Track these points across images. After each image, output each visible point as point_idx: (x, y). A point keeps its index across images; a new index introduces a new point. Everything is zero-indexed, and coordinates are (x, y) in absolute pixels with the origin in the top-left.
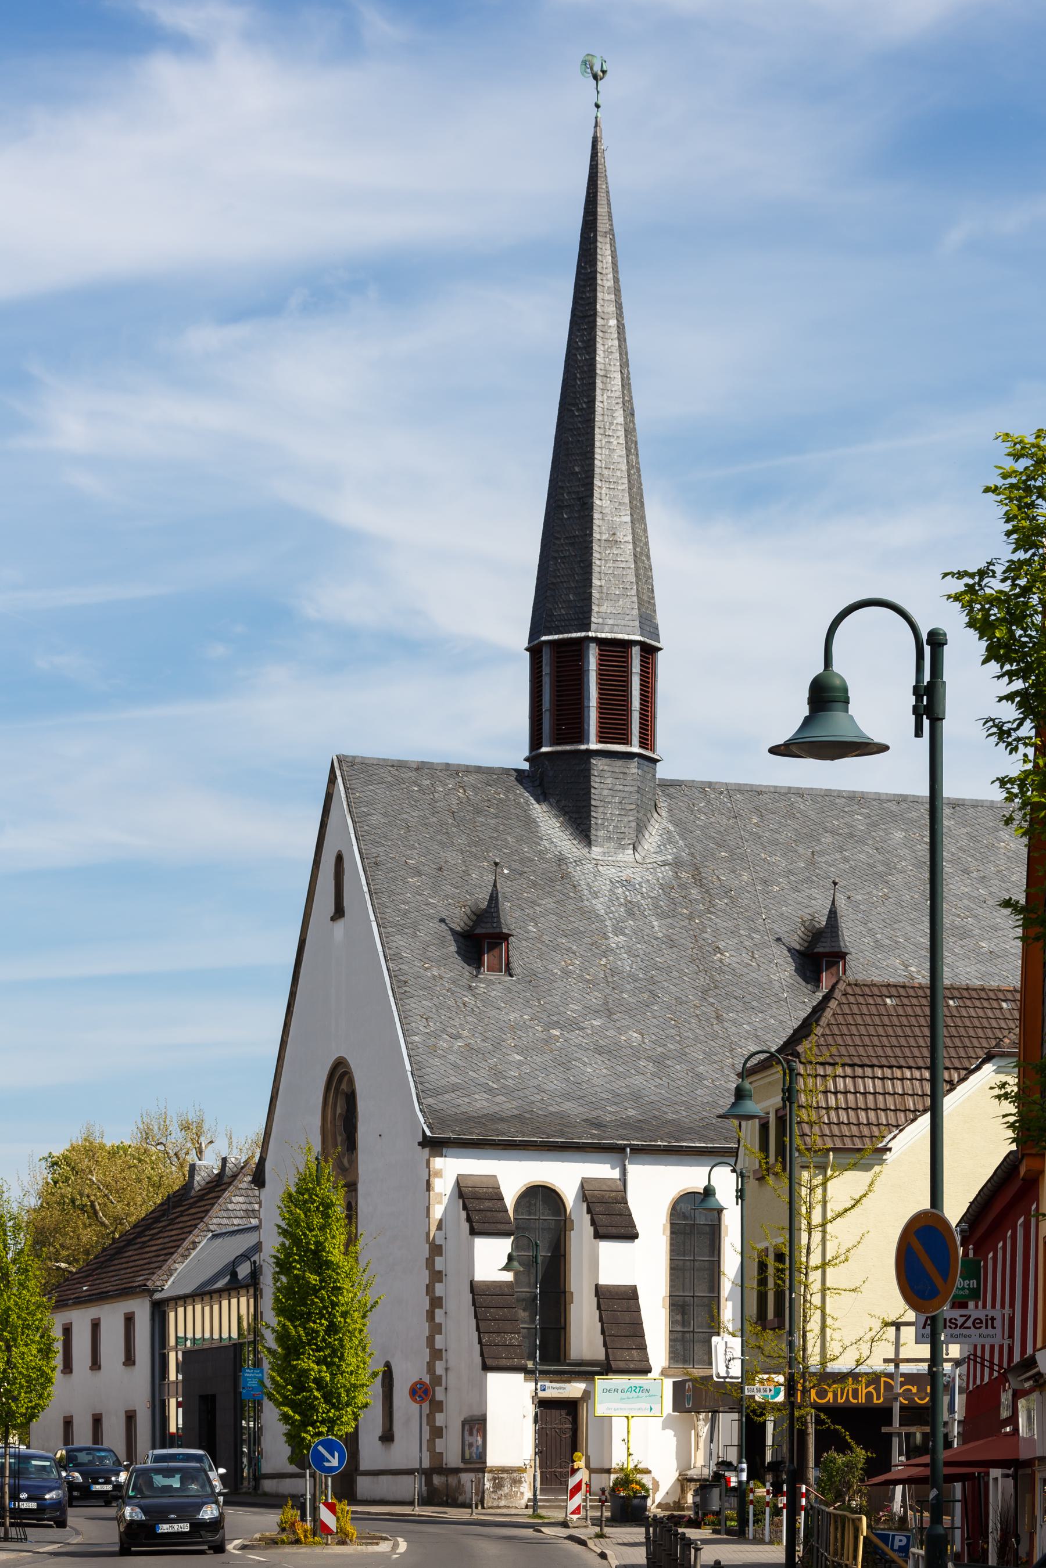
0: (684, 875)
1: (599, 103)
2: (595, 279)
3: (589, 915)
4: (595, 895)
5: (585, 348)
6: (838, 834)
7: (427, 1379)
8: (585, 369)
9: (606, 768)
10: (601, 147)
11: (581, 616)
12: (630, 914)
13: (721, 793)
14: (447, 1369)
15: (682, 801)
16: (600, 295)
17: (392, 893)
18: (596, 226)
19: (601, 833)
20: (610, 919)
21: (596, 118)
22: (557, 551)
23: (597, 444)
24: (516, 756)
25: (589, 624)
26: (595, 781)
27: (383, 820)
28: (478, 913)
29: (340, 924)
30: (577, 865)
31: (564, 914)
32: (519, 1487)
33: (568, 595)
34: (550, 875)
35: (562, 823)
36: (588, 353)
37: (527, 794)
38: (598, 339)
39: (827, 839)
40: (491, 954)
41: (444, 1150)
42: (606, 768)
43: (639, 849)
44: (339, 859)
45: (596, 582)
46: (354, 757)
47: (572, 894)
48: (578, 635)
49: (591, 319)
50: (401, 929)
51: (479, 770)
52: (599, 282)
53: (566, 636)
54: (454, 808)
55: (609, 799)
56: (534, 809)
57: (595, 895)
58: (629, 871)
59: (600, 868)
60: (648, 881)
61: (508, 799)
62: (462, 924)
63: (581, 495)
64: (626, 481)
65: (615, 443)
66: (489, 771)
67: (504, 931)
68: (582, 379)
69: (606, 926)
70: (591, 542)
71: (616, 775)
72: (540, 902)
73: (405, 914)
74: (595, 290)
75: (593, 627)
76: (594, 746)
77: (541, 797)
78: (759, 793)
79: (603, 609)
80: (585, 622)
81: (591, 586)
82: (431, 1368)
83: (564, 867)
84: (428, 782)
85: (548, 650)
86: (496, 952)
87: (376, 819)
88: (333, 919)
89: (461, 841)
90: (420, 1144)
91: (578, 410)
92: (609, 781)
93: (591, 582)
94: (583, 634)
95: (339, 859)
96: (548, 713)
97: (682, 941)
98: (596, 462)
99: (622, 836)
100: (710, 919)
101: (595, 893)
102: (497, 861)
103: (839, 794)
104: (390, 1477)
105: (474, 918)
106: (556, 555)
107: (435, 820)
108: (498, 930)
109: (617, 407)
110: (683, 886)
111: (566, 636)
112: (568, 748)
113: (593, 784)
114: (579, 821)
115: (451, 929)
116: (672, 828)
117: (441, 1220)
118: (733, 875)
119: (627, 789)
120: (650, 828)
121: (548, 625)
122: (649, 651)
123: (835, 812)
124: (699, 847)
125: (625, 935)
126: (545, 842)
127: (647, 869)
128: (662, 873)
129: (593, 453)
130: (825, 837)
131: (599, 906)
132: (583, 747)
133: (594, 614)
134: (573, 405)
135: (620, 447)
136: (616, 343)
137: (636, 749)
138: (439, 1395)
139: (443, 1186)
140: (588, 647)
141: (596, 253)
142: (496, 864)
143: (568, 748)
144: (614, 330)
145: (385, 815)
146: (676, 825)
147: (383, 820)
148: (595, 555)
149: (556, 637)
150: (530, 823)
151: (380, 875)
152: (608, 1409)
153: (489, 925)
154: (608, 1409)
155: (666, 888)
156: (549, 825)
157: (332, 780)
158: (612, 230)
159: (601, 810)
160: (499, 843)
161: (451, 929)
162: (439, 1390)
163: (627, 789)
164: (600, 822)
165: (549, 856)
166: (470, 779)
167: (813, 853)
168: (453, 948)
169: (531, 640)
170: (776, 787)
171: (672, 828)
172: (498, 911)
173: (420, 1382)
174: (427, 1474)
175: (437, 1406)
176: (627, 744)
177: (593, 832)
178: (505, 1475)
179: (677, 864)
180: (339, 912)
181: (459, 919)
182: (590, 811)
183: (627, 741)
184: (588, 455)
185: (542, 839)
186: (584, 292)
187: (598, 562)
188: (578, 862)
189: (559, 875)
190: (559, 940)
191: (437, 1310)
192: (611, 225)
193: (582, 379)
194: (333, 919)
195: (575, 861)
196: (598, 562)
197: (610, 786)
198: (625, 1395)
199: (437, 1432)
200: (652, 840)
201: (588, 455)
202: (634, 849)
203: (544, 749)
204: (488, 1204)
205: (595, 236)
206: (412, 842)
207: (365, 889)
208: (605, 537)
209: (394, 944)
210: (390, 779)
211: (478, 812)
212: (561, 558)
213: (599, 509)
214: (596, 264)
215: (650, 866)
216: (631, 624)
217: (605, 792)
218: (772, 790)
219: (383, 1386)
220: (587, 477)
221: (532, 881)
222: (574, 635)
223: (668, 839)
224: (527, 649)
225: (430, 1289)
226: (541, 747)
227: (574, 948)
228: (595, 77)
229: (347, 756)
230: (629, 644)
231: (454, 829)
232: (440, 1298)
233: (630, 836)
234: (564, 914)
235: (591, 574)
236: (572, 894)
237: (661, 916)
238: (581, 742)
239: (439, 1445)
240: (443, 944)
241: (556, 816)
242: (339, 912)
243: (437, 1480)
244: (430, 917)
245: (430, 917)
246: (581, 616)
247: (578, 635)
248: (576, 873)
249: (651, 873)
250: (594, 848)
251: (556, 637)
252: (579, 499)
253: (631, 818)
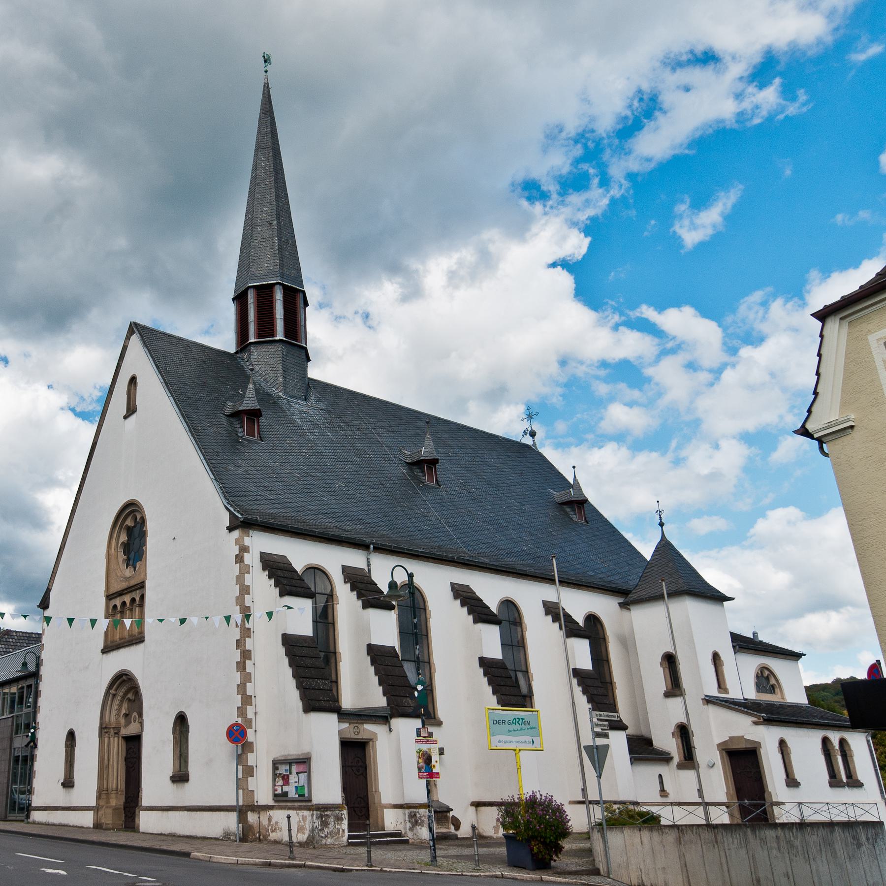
7: (240, 721)
14: (256, 713)
29: (133, 418)
32: (340, 825)
41: (251, 532)
44: (133, 380)
82: (242, 712)
90: (228, 528)
95: (133, 380)
104: (160, 812)
116: (119, 608)
117: (17, 733)
131: (297, 419)
138: (250, 736)
139: (252, 559)
152: (500, 742)
154: (500, 742)
162: (250, 732)
173: (236, 724)
174: (242, 812)
175: (248, 747)
178: (328, 813)
191: (247, 661)
198: (514, 727)
199: (249, 771)
204: (287, 574)
219: (174, 733)
225: (239, 644)
232: (250, 651)
239: (252, 783)
243: (252, 817)
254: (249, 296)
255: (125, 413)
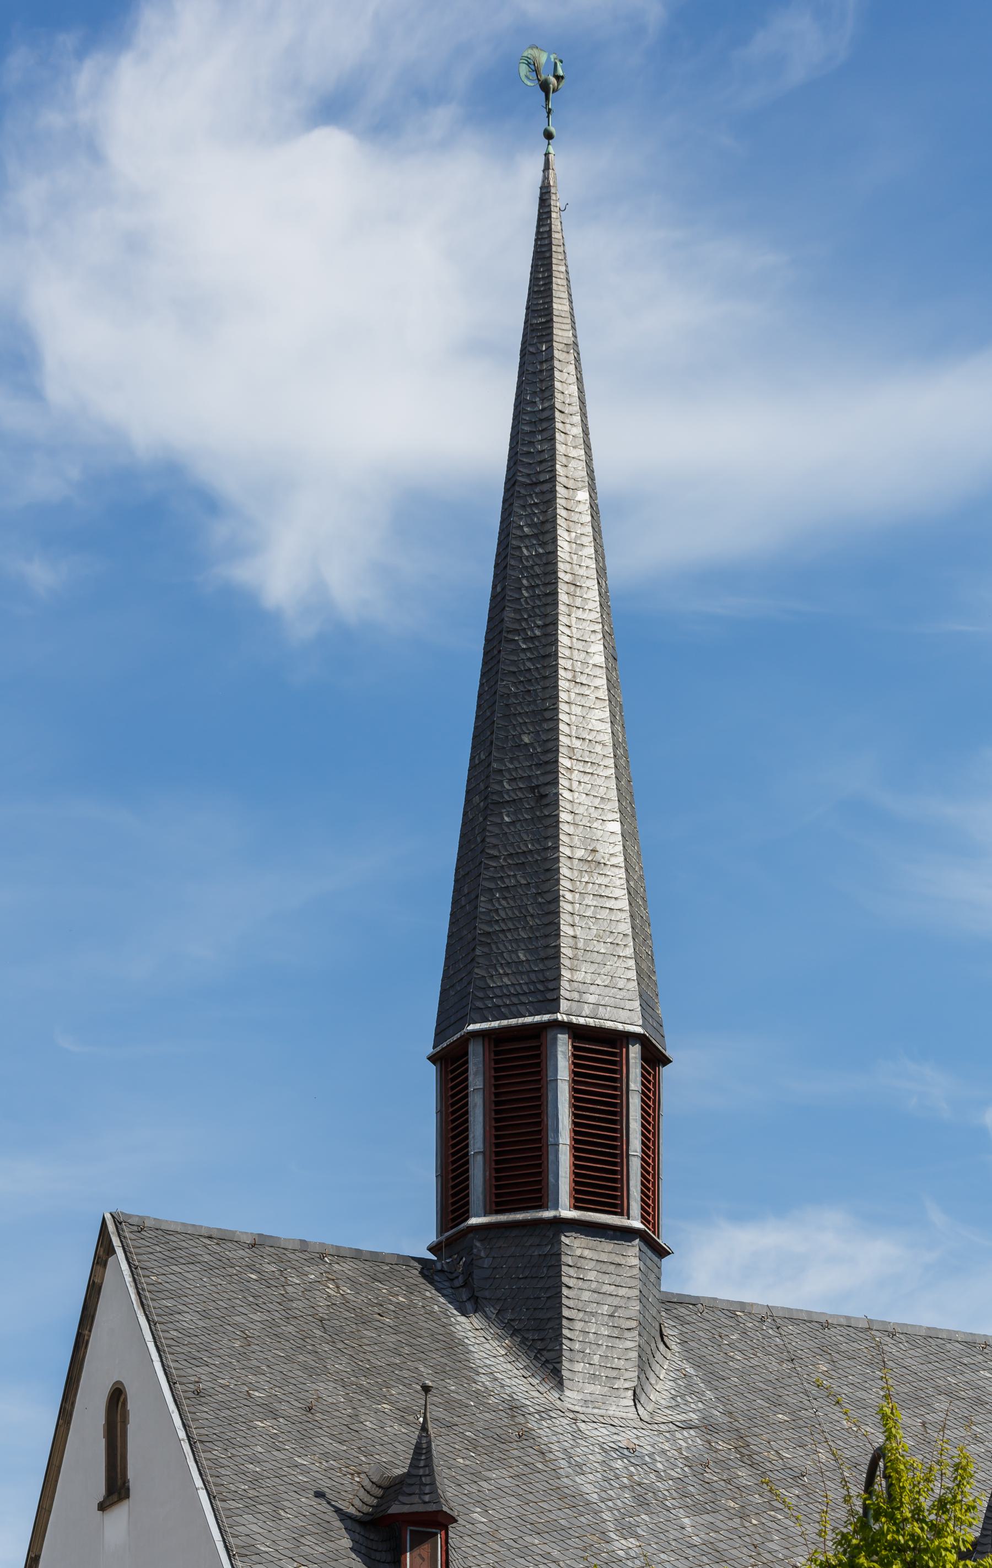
0: (721, 1446)
1: (552, 129)
2: (552, 419)
3: (573, 1500)
4: (579, 1469)
5: (535, 536)
6: (959, 1399)
8: (538, 570)
9: (586, 1253)
10: (557, 202)
11: (540, 987)
12: (642, 1503)
13: (762, 1320)
15: (703, 1329)
16: (560, 448)
17: (230, 1443)
18: (551, 334)
19: (579, 1367)
20: (610, 1509)
21: (547, 155)
22: (492, 879)
23: (563, 696)
24: (417, 1235)
25: (557, 1000)
26: (569, 1276)
27: (201, 1323)
28: (386, 1484)
29: (120, 1513)
30: (543, 1419)
31: (530, 1497)
33: (516, 952)
34: (499, 1431)
35: (509, 1349)
36: (543, 544)
37: (442, 1300)
38: (560, 521)
39: (942, 1404)
40: (417, 1551)
42: (586, 1253)
43: (643, 1398)
44: (117, 1397)
45: (565, 929)
46: (142, 1218)
47: (540, 1466)
48: (537, 1018)
49: (546, 487)
50: (252, 1505)
51: (357, 1255)
52: (559, 425)
53: (513, 1022)
54: (322, 1312)
55: (592, 1308)
56: (459, 1323)
57: (579, 1469)
58: (630, 1434)
59: (582, 1426)
60: (664, 1452)
61: (412, 1305)
62: (357, 1502)
63: (535, 782)
64: (611, 762)
65: (592, 697)
66: (375, 1258)
67: (445, 1509)
68: (531, 587)
69: (604, 1521)
70: (557, 860)
71: (604, 1268)
72: (488, 1474)
73: (256, 1480)
74: (553, 439)
75: (564, 1005)
76: (567, 1213)
77: (469, 1306)
78: (826, 1325)
79: (579, 976)
80: (550, 996)
81: (558, 936)
83: (521, 1419)
84: (272, 1268)
85: (480, 1049)
86: (425, 1549)
87: (188, 1320)
88: (103, 1507)
89: (341, 1366)
91: (525, 640)
92: (592, 1275)
93: (559, 929)
94: (546, 1017)
95: (117, 1397)
96: (480, 1158)
97: (734, 1552)
98: (562, 726)
99: (614, 1374)
100: (775, 1520)
101: (579, 1465)
102: (429, 1383)
103: (950, 1338)
105: (379, 1492)
106: (492, 886)
107: (291, 1329)
108: (433, 1508)
109: (593, 637)
110: (723, 1464)
111: (513, 1022)
112: (520, 1216)
113: (565, 1280)
114: (539, 1345)
115: (338, 1511)
116: (691, 1371)
118: (801, 1452)
119: (622, 1292)
120: (656, 1367)
121: (479, 1004)
122: (655, 1059)
123: (949, 1364)
124: (739, 1403)
125: (637, 1537)
126: (484, 1378)
127: (660, 1432)
128: (685, 1440)
129: (556, 710)
130: (940, 1402)
131: (588, 1486)
132: (548, 1214)
133: (564, 984)
134: (516, 631)
135: (599, 704)
136: (589, 529)
137: (637, 1224)
140: (555, 1040)
141: (552, 377)
142: (426, 1389)
143: (520, 1216)
144: (585, 508)
145: (204, 1315)
146: (697, 1366)
147: (201, 1323)
148: (564, 883)
149: (495, 1024)
150: (454, 1347)
151: (205, 1412)
153: (415, 1499)
155: (698, 1466)
156: (485, 1348)
157: (104, 1250)
158: (575, 344)
159: (578, 1325)
160: (406, 1373)
161: (338, 1511)
163: (622, 1292)
164: (577, 1346)
165: (492, 1400)
166: (346, 1267)
167: (924, 1424)
168: (347, 1542)
169: (440, 1034)
170: (848, 1318)
171: (691, 1371)
172: (431, 1474)
176: (621, 1214)
177: (566, 1364)
179: (708, 1428)
180: (117, 1489)
181: (353, 1497)
182: (560, 1326)
183: (619, 1208)
184: (548, 715)
185: (478, 1374)
186: (531, 443)
187: (569, 896)
188: (545, 1413)
189: (513, 1432)
190: (528, 1538)
192: (575, 336)
193: (531, 587)
194: (103, 1507)
195: (539, 1412)
196: (569, 896)
197: (594, 1285)
200: (662, 1389)
201: (548, 715)
202: (635, 1398)
203: (473, 1221)
205: (550, 348)
206: (255, 1362)
207: (182, 1434)
208: (580, 853)
209: (241, 1529)
210: (207, 1258)
211: (365, 1322)
212: (501, 890)
213: (568, 806)
214: (552, 396)
215: (663, 1427)
216: (629, 1005)
217: (586, 1296)
218: (843, 1322)
220: (546, 752)
221: (469, 1440)
222: (529, 1020)
223: (686, 1389)
224: (432, 1059)
226: (467, 1219)
227: (555, 1553)
228: (545, 86)
229: (130, 1216)
230: (625, 1038)
231: (327, 1347)
233: (628, 1375)
234: (530, 1497)
235: (557, 913)
236: (540, 1466)
237: (696, 1509)
238: (542, 1206)
240: (327, 1533)
241: (500, 1338)
242: (117, 1489)
244: (301, 1489)
245: (301, 1489)
246: (540, 987)
247: (537, 1018)
248: (543, 1431)
249: (668, 1440)
250: (567, 1393)
251: (495, 1024)
252: (532, 789)
253: (630, 1344)
254: (472, 1068)
255: (99, 1490)
